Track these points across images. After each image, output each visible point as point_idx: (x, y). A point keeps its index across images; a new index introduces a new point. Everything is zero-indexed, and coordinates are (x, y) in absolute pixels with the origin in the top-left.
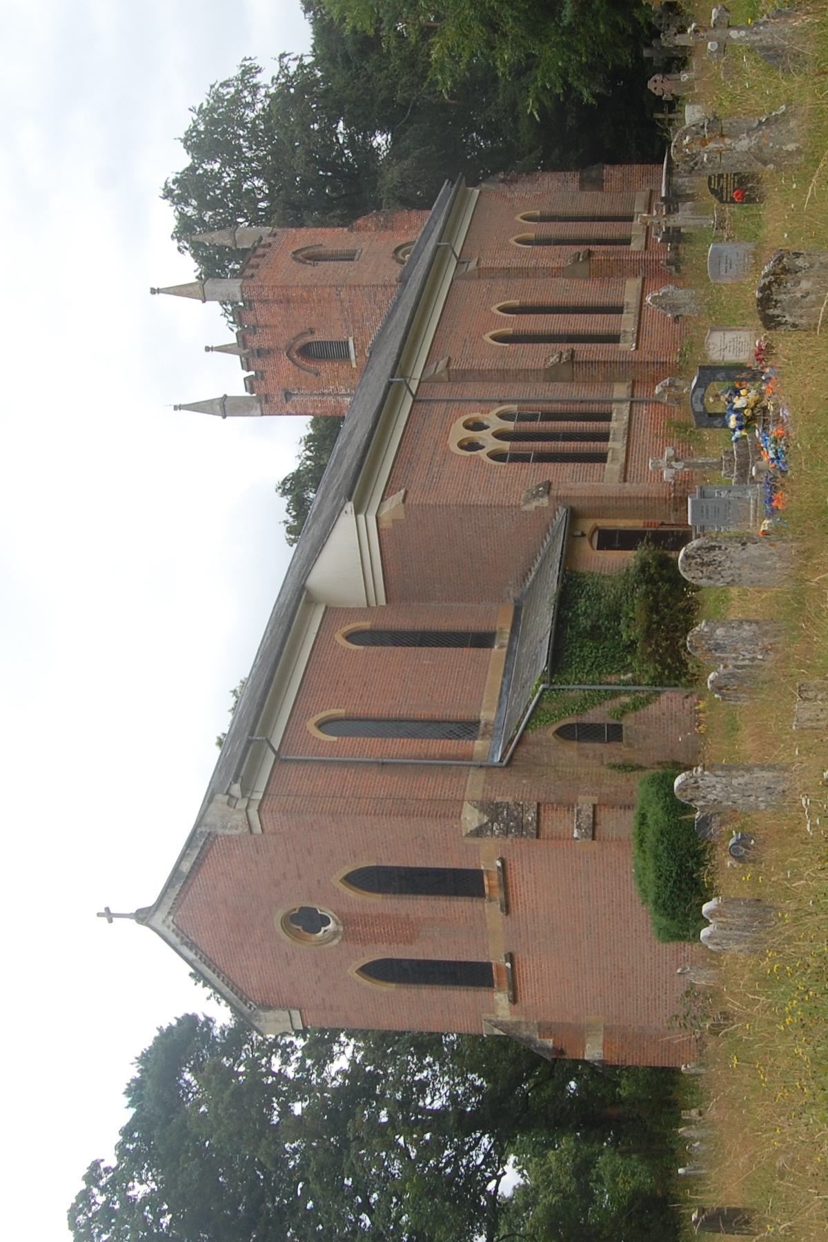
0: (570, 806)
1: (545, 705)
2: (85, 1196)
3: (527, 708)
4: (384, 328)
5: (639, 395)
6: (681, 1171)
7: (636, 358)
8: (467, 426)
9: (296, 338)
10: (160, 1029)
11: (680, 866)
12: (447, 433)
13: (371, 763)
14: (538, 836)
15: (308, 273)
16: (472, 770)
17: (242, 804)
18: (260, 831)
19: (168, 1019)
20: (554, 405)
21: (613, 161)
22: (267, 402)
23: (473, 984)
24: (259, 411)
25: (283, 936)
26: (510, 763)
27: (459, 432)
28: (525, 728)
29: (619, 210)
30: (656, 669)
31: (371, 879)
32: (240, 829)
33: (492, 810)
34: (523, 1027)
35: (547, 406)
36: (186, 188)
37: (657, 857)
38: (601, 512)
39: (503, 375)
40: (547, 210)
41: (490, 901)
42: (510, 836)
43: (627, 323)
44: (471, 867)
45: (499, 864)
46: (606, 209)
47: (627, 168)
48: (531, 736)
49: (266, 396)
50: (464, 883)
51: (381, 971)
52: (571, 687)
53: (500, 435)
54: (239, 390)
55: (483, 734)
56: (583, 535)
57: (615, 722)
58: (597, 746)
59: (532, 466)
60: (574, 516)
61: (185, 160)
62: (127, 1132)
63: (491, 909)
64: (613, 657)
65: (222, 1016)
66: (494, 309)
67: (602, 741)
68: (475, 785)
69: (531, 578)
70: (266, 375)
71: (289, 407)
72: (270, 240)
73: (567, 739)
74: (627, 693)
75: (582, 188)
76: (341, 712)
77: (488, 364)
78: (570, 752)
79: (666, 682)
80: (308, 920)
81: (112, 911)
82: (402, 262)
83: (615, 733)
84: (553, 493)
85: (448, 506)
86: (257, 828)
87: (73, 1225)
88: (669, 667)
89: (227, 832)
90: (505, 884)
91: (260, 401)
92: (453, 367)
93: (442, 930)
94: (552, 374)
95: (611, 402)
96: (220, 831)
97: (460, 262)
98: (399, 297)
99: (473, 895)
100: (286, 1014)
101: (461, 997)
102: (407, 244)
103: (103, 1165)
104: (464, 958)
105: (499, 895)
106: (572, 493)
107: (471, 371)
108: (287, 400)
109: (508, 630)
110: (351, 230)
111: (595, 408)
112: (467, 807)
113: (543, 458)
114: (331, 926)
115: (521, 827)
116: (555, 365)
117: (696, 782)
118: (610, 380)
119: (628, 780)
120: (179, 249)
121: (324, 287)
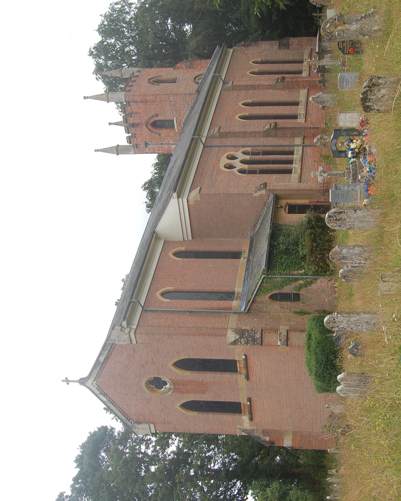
0: (276, 331)
1: (264, 285)
3: (256, 286)
4: (190, 113)
8: (228, 158)
10: (90, 433)
11: (327, 358)
12: (219, 161)
15: (155, 88)
16: (231, 314)
17: (127, 331)
22: (137, 148)
24: (134, 152)
26: (249, 311)
27: (224, 161)
28: (256, 295)
29: (297, 58)
30: (315, 268)
33: (241, 332)
34: (255, 431)
35: (265, 149)
36: (100, 51)
37: (316, 354)
38: (289, 196)
39: (244, 134)
40: (264, 59)
41: (240, 374)
42: (249, 344)
43: (301, 110)
45: (244, 357)
47: (300, 39)
48: (258, 299)
49: (136, 145)
50: (228, 366)
51: (190, 406)
52: (276, 276)
53: (243, 162)
54: (124, 142)
55: (236, 298)
56: (282, 207)
57: (296, 292)
58: (289, 303)
59: (258, 175)
60: (277, 198)
61: (98, 38)
62: (76, 479)
63: (241, 378)
64: (295, 263)
65: (118, 427)
66: (240, 104)
67: (291, 301)
68: (233, 321)
69: (258, 227)
71: (147, 150)
72: (138, 74)
73: (275, 300)
74: (302, 279)
75: (280, 48)
76: (172, 288)
77: (237, 129)
78: (276, 306)
80: (157, 383)
81: (69, 379)
82: (198, 83)
83: (297, 297)
84: (268, 188)
85: (220, 194)
86: (134, 341)
88: (321, 267)
89: (121, 343)
90: (247, 367)
91: (134, 147)
92: (222, 131)
93: (219, 388)
94: (267, 134)
95: (294, 146)
96: (117, 343)
97: (224, 83)
98: (197, 99)
99: (232, 371)
102: (200, 75)
103: (65, 495)
104: (228, 400)
105: (244, 371)
107: (229, 133)
109: (248, 251)
110: (174, 69)
111: (287, 149)
113: (263, 172)
114: (168, 386)
115: (254, 340)
116: (268, 130)
117: (334, 319)
118: (293, 136)
119: (303, 319)
120: (96, 79)
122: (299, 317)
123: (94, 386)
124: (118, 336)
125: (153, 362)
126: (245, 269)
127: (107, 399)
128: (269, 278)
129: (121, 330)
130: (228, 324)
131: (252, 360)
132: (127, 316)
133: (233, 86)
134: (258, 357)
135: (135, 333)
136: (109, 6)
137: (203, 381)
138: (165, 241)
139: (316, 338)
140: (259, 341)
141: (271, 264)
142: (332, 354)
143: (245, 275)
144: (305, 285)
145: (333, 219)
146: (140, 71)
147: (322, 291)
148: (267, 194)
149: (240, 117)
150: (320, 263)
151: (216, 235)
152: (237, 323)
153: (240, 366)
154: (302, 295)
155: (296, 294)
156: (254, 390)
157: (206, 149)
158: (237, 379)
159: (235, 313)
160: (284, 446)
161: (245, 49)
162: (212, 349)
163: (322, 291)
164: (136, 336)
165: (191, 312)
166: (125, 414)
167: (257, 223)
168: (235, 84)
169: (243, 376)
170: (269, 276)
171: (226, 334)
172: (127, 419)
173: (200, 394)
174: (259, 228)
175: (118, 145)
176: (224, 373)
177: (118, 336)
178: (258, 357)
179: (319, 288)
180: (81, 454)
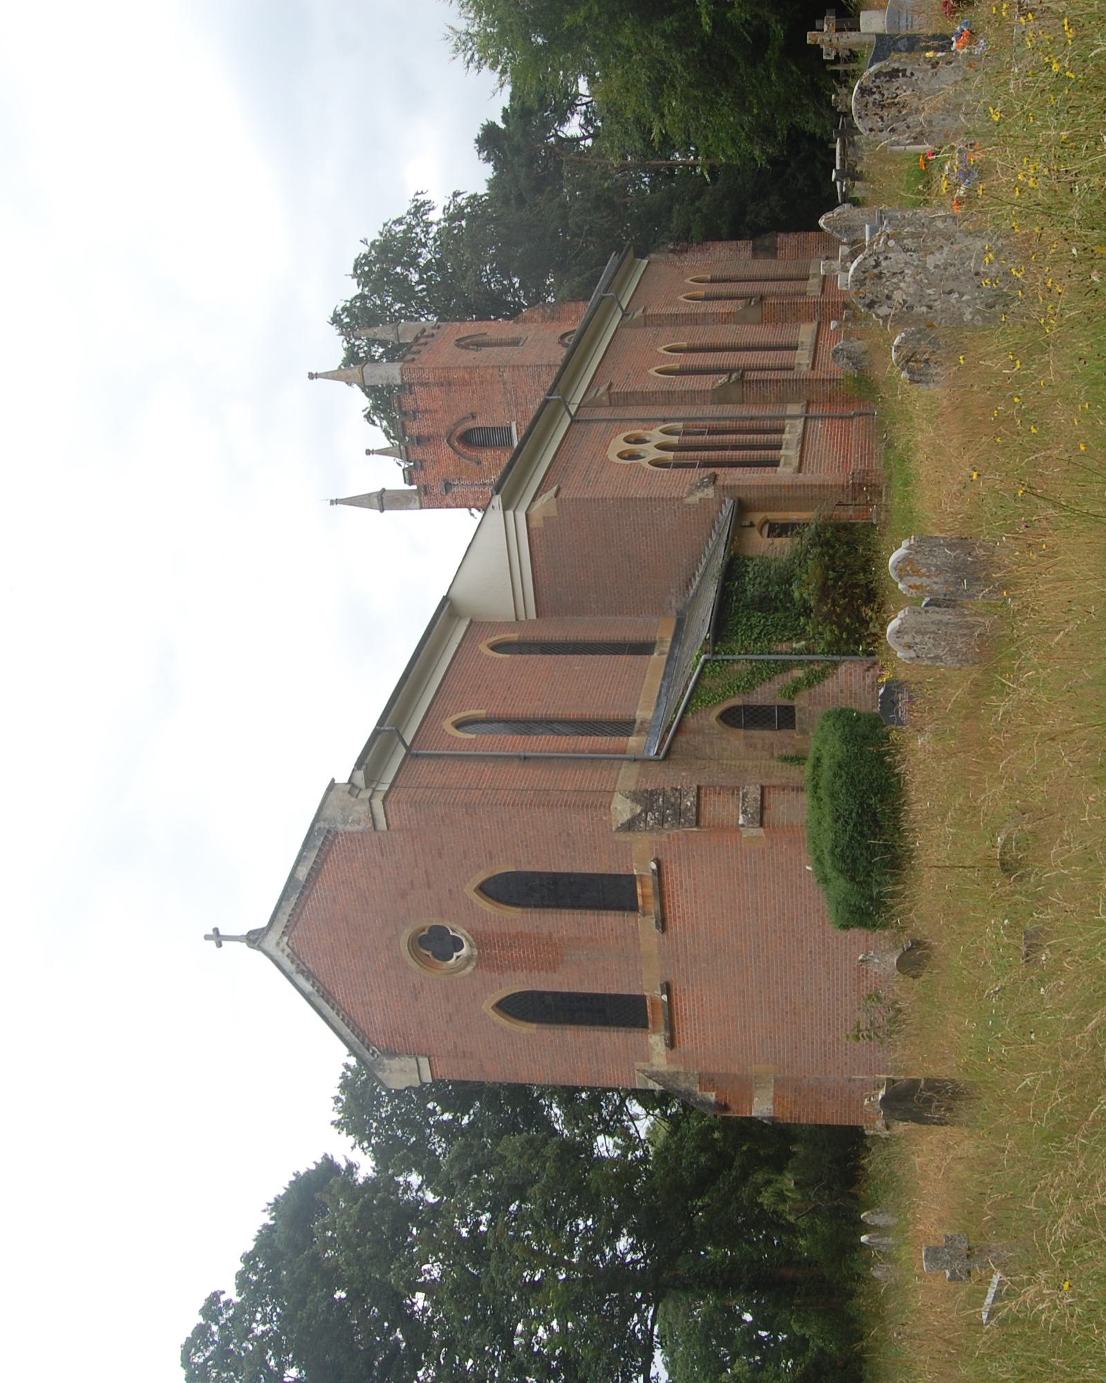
0: (734, 790)
1: (706, 682)
2: (201, 1331)
6: (864, 1239)
7: (811, 375)
8: (627, 440)
11: (861, 804)
14: (697, 824)
15: (469, 357)
17: (366, 794)
19: (307, 1162)
20: (722, 423)
21: (787, 230)
22: (426, 494)
24: (418, 504)
25: (411, 962)
26: (668, 755)
29: (793, 272)
30: (832, 631)
31: (512, 889)
32: (363, 824)
33: (646, 799)
34: (682, 1078)
35: (714, 424)
37: (833, 795)
40: (718, 274)
41: (644, 915)
42: (666, 826)
45: (654, 866)
46: (780, 272)
47: (802, 235)
48: (692, 722)
49: (425, 487)
50: (609, 893)
51: (523, 1007)
52: (736, 657)
53: (661, 447)
56: (752, 525)
57: (785, 702)
58: (767, 734)
60: (742, 508)
61: (352, 289)
62: (248, 1258)
63: (646, 925)
64: (784, 626)
65: (366, 1167)
66: (661, 350)
67: (773, 729)
68: (628, 777)
70: (426, 465)
71: (449, 500)
72: (435, 331)
74: (800, 663)
75: (755, 256)
76: (481, 713)
77: (651, 387)
78: (736, 739)
79: (844, 649)
80: (437, 944)
81: (221, 933)
83: (785, 718)
84: (719, 483)
85: (604, 500)
86: (382, 825)
87: (186, 1361)
88: (846, 628)
89: (349, 828)
90: (661, 893)
92: (614, 390)
93: (592, 954)
94: (720, 396)
95: (784, 418)
96: (340, 827)
97: (625, 314)
99: (634, 1025)
101: (610, 1039)
103: (223, 1298)
104: (614, 990)
105: (653, 907)
107: (633, 393)
109: (670, 639)
111: (767, 424)
114: (464, 952)
115: (679, 813)
117: (877, 264)
118: (783, 400)
123: (283, 951)
124: (343, 809)
125: (428, 883)
126: (661, 675)
127: (313, 986)
135: (384, 801)
136: (381, 228)
138: (471, 621)
139: (833, 757)
140: (691, 816)
142: (876, 795)
145: (871, 99)
151: (593, 606)
153: (644, 891)
154: (800, 710)
155: (787, 707)
157: (577, 426)
159: (635, 760)
161: (676, 258)
166: (357, 1030)
167: (694, 575)
168: (649, 312)
169: (652, 921)
170: (719, 657)
172: (363, 1043)
173: (543, 973)
174: (698, 588)
175: (384, 490)
176: (604, 912)
177: (343, 809)
179: (842, 691)
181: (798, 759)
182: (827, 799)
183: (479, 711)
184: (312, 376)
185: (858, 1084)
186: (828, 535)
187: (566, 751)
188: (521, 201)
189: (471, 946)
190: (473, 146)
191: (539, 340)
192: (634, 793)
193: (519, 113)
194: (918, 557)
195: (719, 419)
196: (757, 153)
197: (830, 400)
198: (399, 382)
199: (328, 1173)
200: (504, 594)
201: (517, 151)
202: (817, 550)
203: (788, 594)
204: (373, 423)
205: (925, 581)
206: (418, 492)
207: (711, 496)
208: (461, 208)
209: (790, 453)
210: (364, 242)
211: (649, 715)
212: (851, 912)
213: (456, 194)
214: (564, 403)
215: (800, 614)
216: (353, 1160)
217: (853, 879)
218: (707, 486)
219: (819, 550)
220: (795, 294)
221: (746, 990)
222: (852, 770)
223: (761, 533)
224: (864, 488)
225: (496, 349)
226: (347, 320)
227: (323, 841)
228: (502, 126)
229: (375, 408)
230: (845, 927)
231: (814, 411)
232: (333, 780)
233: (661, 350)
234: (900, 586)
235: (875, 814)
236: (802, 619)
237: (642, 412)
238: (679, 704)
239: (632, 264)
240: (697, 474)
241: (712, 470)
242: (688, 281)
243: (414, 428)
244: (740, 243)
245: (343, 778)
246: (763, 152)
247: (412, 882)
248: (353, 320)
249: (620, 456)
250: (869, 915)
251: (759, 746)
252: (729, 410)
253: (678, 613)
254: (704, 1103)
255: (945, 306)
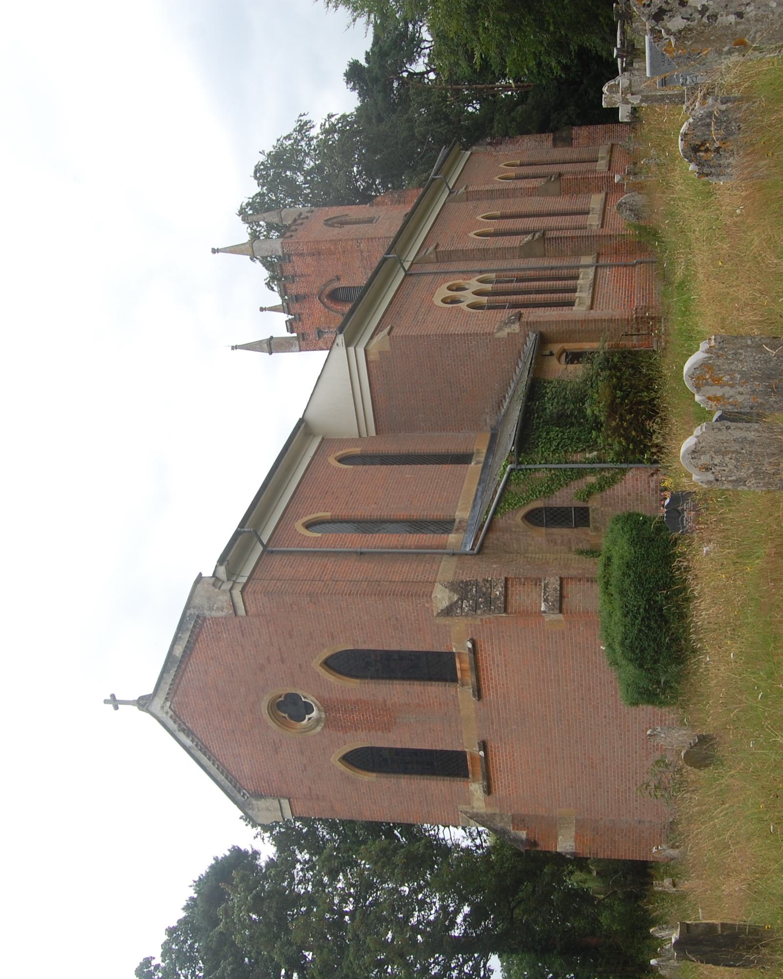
0: (537, 581)
1: (512, 488)
3: (496, 491)
5: (602, 261)
6: (653, 962)
7: (600, 232)
8: (450, 288)
9: (326, 285)
10: (216, 859)
11: (648, 601)
13: (350, 553)
14: (505, 611)
15: (335, 233)
16: (445, 557)
17: (227, 586)
18: (244, 613)
22: (304, 339)
23: (448, 775)
24: (298, 348)
25: (270, 722)
29: (585, 156)
30: (620, 443)
31: (351, 664)
32: (225, 611)
33: (462, 588)
34: (498, 819)
35: (521, 273)
37: (622, 592)
40: (525, 159)
41: (463, 685)
42: (479, 612)
44: (443, 649)
45: (470, 645)
46: (575, 156)
47: (592, 128)
48: (501, 522)
49: (303, 334)
50: (434, 667)
51: (365, 760)
52: (537, 466)
53: (478, 293)
55: (457, 530)
56: (552, 354)
57: (581, 504)
58: (565, 531)
60: (543, 340)
61: (254, 188)
63: (464, 694)
65: (267, 851)
68: (447, 569)
72: (309, 215)
73: (536, 524)
74: (593, 471)
75: (555, 145)
76: (328, 515)
77: (470, 246)
78: (539, 536)
79: (631, 458)
81: (117, 698)
83: (580, 517)
84: (523, 319)
85: (428, 336)
86: (241, 611)
88: (633, 440)
89: (214, 614)
90: (476, 668)
92: (441, 249)
93: (419, 716)
95: (578, 267)
96: (207, 613)
100: (276, 802)
103: (154, 963)
104: (440, 747)
105: (470, 679)
106: (542, 319)
108: (320, 338)
109: (485, 451)
110: (372, 206)
111: (565, 272)
112: (438, 587)
114: (314, 714)
115: (489, 602)
121: (347, 240)
122: (588, 560)
123: (167, 713)
124: (209, 598)
125: (282, 658)
126: (477, 481)
127: (192, 741)
128: (521, 470)
129: (213, 585)
130: (437, 575)
131: (489, 654)
132: (228, 558)
133: (467, 192)
134: (500, 644)
135: (242, 592)
137: (385, 701)
141: (525, 441)
143: (477, 490)
144: (600, 487)
146: (312, 211)
147: (637, 500)
148: (522, 333)
149: (476, 234)
150: (630, 432)
151: (422, 425)
152: (455, 574)
153: (462, 665)
154: (593, 511)
155: (582, 508)
156: (492, 723)
157: (410, 279)
158: (457, 697)
159: (453, 554)
160: (558, 850)
161: (493, 149)
162: (402, 626)
163: (637, 500)
164: (245, 597)
165: (361, 553)
166: (230, 777)
167: (504, 397)
168: (470, 189)
169: (469, 691)
170: (523, 467)
171: (432, 592)
172: (235, 787)
173: (380, 733)
174: (508, 408)
175: (272, 337)
176: (430, 683)
178: (500, 644)
179: (629, 494)
180: (195, 896)
181: (593, 552)
182: (616, 596)
183: (325, 514)
184: (214, 251)
185: (647, 825)
186: (616, 360)
187: (396, 547)
188: (380, 119)
189: (319, 710)
190: (342, 79)
191: (387, 216)
192: (452, 584)
193: (378, 53)
194: (720, 362)
195: (524, 269)
196: (553, 64)
197: (617, 252)
198: (280, 253)
199: (238, 862)
200: (349, 415)
201: (376, 80)
202: (603, 374)
203: (581, 411)
204: (272, 289)
205: (728, 391)
206: (298, 338)
207: (517, 331)
208: (334, 125)
209: (583, 295)
210: (262, 153)
211: (466, 515)
212: (640, 693)
213: (330, 116)
214: (399, 261)
215: (592, 429)
216: (256, 848)
217: (641, 666)
218: (514, 323)
219: (608, 372)
220: (588, 171)
221: (549, 744)
222: (639, 570)
223: (559, 359)
224: (646, 322)
225: (355, 226)
226: (251, 212)
227: (194, 627)
228: (366, 65)
229: (273, 278)
230: (635, 704)
231: (602, 261)
232: (200, 574)
233: (479, 218)
234: (697, 398)
235: (661, 610)
236: (594, 432)
237: (462, 266)
238: (490, 507)
239: (459, 153)
240: (507, 313)
241: (517, 310)
242: (502, 165)
243: (293, 289)
244: (543, 135)
245: (208, 573)
246: (559, 62)
247: (268, 658)
248: (252, 212)
249: (444, 301)
250: (657, 695)
251: (559, 542)
252: (533, 262)
253: (492, 429)
254: (516, 840)
255: (760, 12)
